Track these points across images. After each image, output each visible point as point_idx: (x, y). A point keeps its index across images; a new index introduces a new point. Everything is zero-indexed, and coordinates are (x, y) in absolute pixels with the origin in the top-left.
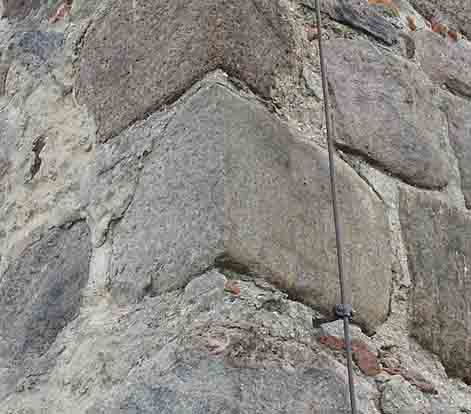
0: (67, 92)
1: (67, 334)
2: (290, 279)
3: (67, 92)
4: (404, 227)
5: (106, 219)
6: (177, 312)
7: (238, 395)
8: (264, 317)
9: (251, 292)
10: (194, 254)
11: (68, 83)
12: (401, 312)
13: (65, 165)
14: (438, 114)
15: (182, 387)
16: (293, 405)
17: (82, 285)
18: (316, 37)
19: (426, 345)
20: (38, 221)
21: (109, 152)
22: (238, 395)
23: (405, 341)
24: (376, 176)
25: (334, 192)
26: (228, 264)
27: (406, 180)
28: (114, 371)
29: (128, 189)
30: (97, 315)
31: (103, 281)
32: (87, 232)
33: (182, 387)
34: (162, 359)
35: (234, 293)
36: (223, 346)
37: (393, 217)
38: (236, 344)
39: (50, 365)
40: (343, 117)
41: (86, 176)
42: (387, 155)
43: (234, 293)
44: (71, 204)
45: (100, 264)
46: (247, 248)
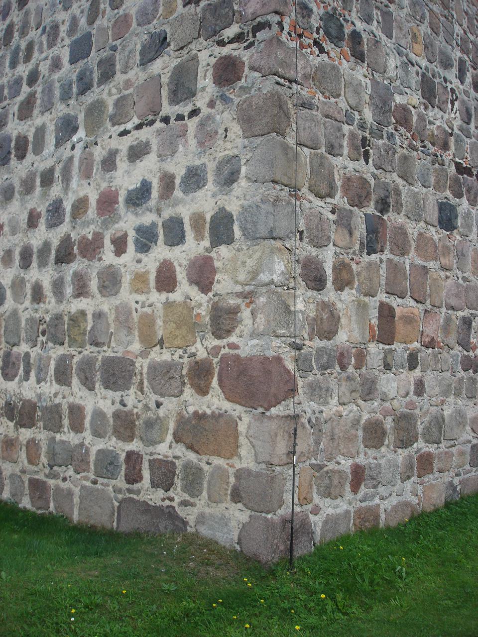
0: (234, 119)
1: (235, 185)
2: (285, 182)
3: (234, 119)
4: (310, 163)
5: (246, 160)
6: (262, 188)
7: (274, 211)
8: (280, 193)
9: (278, 187)
10: (266, 178)
11: (235, 117)
12: (307, 184)
13: (234, 140)
14: (322, 125)
15: (263, 206)
16: (330, 554)
17: (239, 174)
18: (296, 113)
19: (311, 191)
20: (227, 152)
21: (246, 141)
22: (274, 211)
23: (307, 190)
24: (305, 149)
25: (297, 155)
26: (274, 182)
27: (312, 149)
28: (247, 197)
29: (251, 154)
30: (243, 182)
31: (244, 175)
32: (240, 160)
33: (263, 206)
34: (258, 198)
35: (274, 188)
36: (272, 200)
37: (308, 160)
38: (275, 200)
39: (231, 191)
40: (302, 453)
41: (240, 145)
42: (309, 143)
43: (274, 188)
44: (236, 152)
45: (243, 170)
46: (278, 178)
